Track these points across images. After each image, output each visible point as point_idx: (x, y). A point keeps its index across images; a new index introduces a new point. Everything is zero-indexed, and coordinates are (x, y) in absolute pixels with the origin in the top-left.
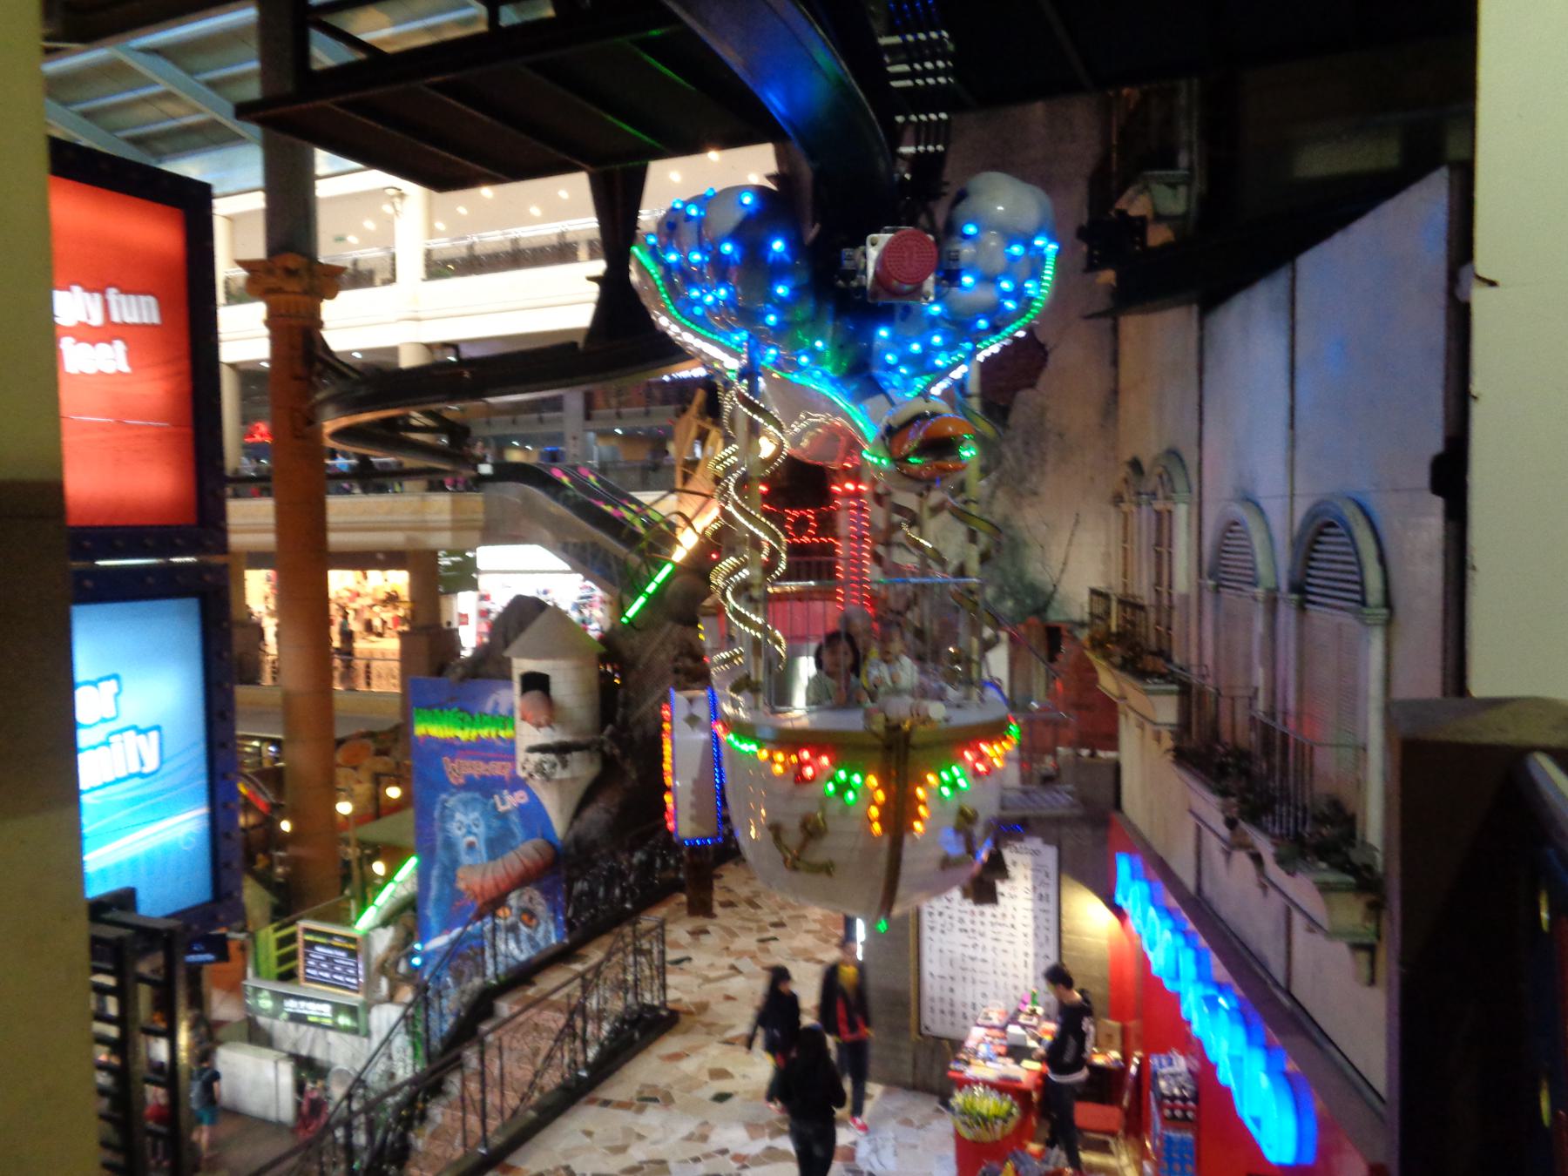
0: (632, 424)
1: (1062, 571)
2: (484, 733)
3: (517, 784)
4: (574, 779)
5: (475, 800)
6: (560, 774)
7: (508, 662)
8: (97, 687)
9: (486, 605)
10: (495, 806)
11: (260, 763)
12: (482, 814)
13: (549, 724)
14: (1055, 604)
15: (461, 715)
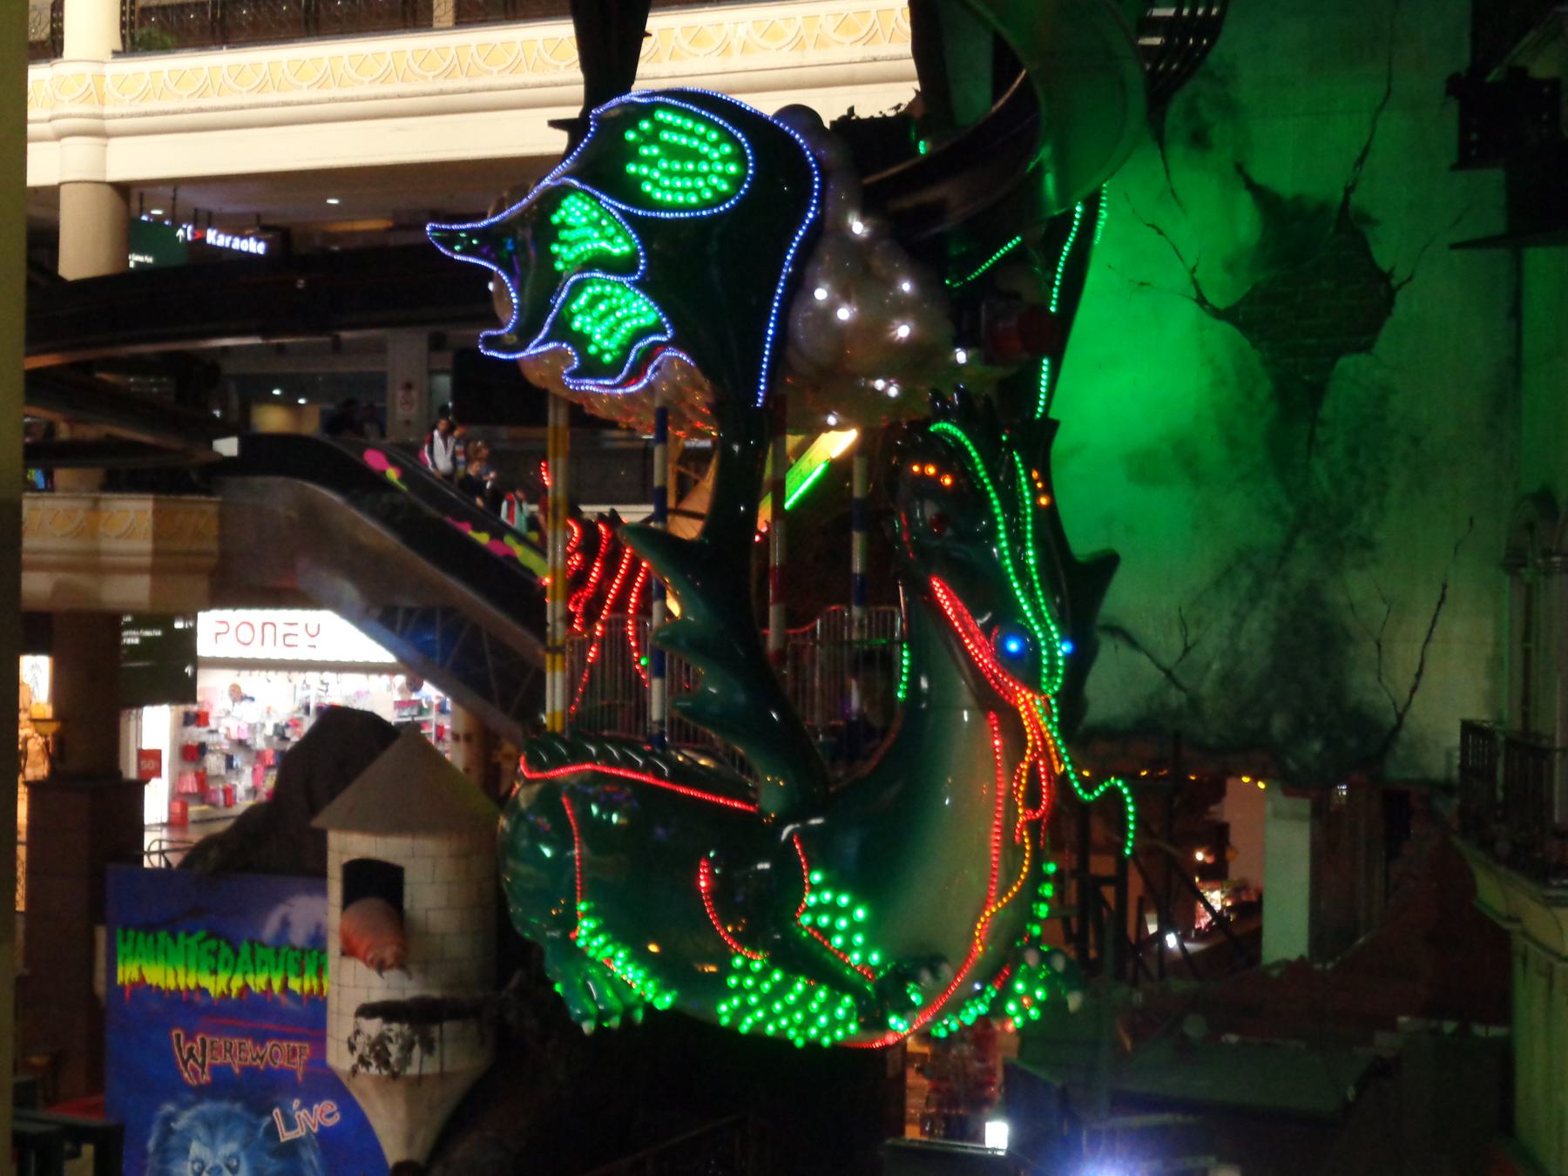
1: (1414, 690)
2: (258, 982)
4: (442, 1076)
5: (228, 1117)
7: (320, 839)
8: (1107, 563)
9: (197, 734)
10: (272, 1131)
12: (245, 1146)
13: (401, 964)
14: (1400, 752)
15: (212, 944)
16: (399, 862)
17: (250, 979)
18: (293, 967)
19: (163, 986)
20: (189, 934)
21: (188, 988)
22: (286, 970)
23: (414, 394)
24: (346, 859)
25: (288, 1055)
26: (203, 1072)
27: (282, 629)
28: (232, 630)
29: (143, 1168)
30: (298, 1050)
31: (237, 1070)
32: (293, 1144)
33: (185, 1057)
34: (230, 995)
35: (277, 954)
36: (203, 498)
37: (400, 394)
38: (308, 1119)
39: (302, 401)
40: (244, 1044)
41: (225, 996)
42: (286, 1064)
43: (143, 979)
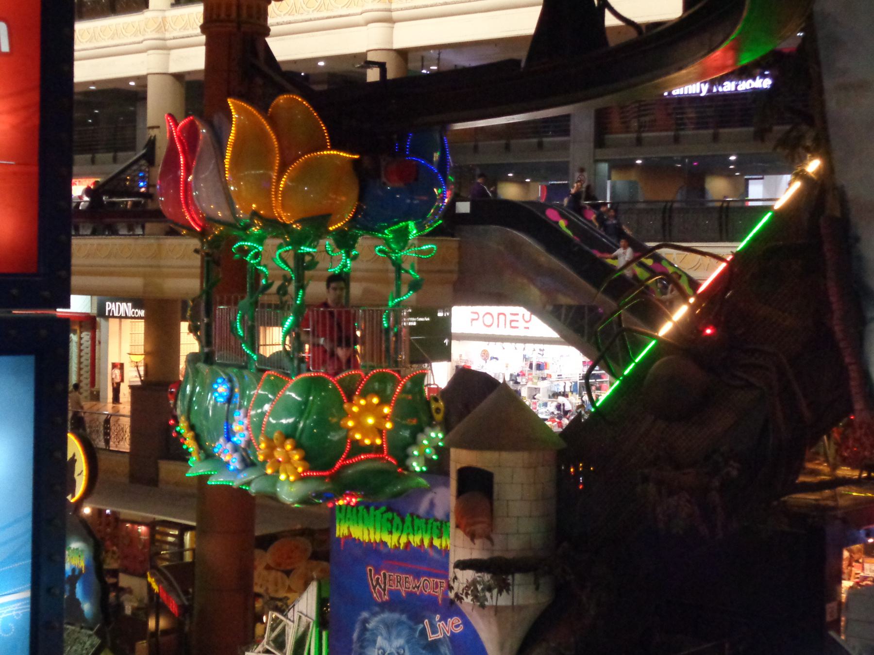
0: (661, 152)
2: (415, 540)
3: (450, 608)
5: (400, 623)
6: (494, 599)
10: (423, 632)
11: (181, 555)
12: (408, 642)
15: (389, 515)
16: (490, 470)
17: (411, 538)
18: (436, 531)
19: (362, 540)
20: (377, 508)
21: (375, 542)
22: (431, 533)
23: (585, 174)
24: (459, 467)
25: (433, 588)
26: (385, 594)
27: (509, 318)
28: (481, 319)
29: (351, 650)
30: (439, 584)
31: (404, 594)
32: (436, 642)
33: (374, 584)
34: (399, 547)
35: (427, 523)
36: (449, 238)
37: (577, 174)
38: (444, 626)
39: (528, 180)
40: (408, 577)
41: (397, 548)
42: (432, 592)
43: (350, 535)
